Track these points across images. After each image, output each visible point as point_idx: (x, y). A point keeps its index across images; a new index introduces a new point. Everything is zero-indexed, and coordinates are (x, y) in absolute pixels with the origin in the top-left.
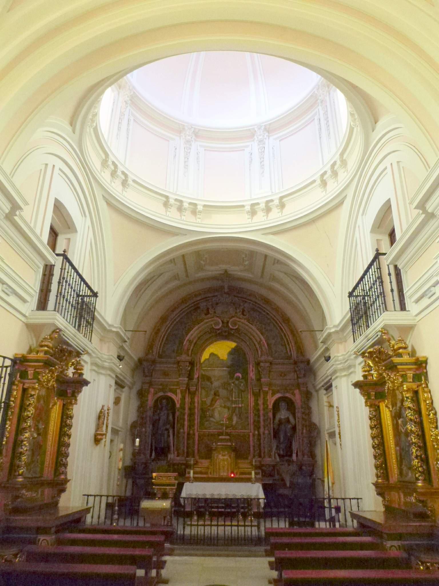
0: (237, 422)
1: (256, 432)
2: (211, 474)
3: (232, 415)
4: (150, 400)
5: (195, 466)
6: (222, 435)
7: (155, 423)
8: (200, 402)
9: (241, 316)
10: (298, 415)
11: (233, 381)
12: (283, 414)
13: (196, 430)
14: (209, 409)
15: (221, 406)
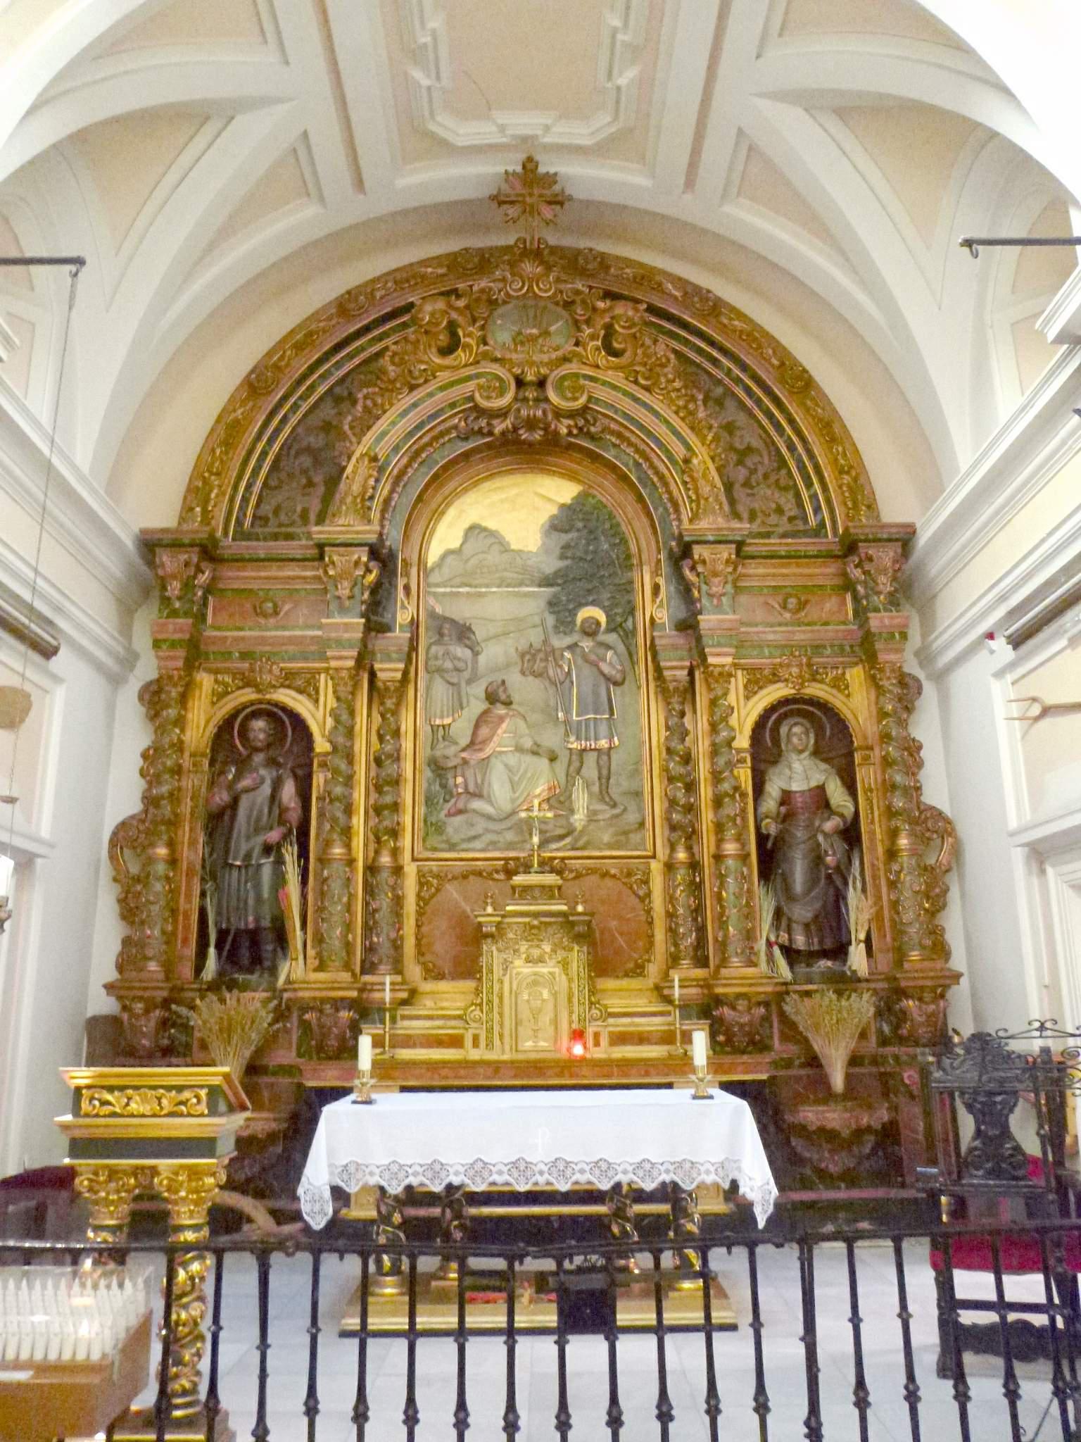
0: (592, 817)
1: (682, 855)
2: (476, 1043)
3: (570, 781)
4: (200, 722)
5: (406, 1011)
6: (527, 868)
7: (219, 822)
8: (424, 730)
9: (602, 359)
10: (866, 775)
11: (568, 640)
12: (800, 773)
13: (407, 855)
14: (465, 762)
15: (519, 749)
